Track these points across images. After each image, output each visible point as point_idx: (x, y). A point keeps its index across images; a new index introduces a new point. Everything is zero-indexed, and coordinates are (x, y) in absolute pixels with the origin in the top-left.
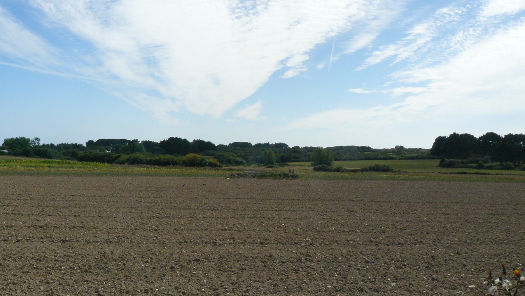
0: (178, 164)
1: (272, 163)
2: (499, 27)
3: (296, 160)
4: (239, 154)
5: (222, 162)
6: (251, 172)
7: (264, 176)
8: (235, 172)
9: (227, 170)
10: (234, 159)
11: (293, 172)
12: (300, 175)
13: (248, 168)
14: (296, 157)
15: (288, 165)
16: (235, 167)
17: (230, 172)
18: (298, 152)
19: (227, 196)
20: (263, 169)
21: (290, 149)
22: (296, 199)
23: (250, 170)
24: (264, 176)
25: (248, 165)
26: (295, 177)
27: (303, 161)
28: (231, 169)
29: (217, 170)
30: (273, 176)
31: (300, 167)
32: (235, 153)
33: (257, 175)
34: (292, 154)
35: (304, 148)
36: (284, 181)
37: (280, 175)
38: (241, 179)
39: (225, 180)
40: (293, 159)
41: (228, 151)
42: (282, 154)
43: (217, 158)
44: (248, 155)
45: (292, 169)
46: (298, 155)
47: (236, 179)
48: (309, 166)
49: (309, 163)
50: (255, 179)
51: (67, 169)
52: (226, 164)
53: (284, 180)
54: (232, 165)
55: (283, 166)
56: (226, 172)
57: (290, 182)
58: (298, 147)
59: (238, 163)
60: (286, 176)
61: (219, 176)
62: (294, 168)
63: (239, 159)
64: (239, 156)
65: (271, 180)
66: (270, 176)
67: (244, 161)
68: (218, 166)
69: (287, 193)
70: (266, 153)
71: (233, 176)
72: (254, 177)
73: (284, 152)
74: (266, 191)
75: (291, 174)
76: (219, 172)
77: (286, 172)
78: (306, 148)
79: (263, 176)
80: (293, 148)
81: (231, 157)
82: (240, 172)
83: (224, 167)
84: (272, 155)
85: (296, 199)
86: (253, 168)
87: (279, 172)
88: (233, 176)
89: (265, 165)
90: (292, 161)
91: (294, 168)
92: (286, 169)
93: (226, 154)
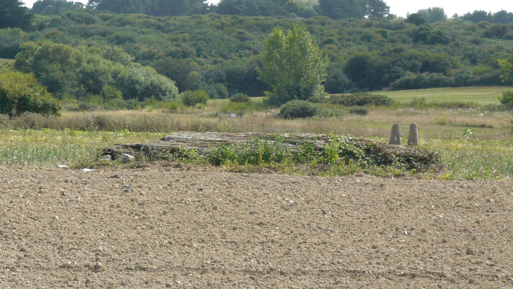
0: (132, 147)
1: (306, 94)
2: (35, 74)
3: (426, 76)
4: (144, 49)
5: (54, 87)
6: (199, 136)
7: (266, 158)
8: (122, 138)
9: (84, 127)
10: (115, 75)
11: (412, 140)
12: (445, 157)
13: (185, 118)
14: (428, 66)
15: (384, 103)
16: (123, 114)
17: (98, 140)
18: (438, 39)
19: (82, 257)
20: (258, 122)
21: (399, 25)
22: (427, 274)
23: (195, 128)
24: (266, 158)
25: (188, 102)
26: (420, 162)
27: (462, 83)
28: (101, 124)
29: (32, 126)
30: (315, 158)
31: (448, 114)
32: (120, 41)
33: (230, 150)
34: (409, 49)
35: (468, 17)
36: (366, 182)
37: (348, 155)
38: (154, 170)
39: (72, 175)
40: (412, 76)
41: (87, 35)
42: (361, 50)
43: (36, 66)
44: (185, 55)
45: (405, 122)
46: (431, 53)
47: (126, 175)
48: (491, 109)
49: (493, 96)
50: (222, 173)
51: (89, 115)
52: (78, 95)
53: (367, 178)
54: (107, 99)
55: (360, 106)
56: (79, 135)
57: (396, 186)
58: (437, 14)
59: (135, 93)
60: (379, 157)
61: (42, 157)
62: (414, 119)
63: (144, 74)
64: (146, 59)
65: (298, 177)
66: (297, 159)
67: (169, 84)
68: (36, 109)
69: (380, 242)
70: (275, 43)
71: (114, 155)
72: (217, 162)
73: (367, 38)
74: (275, 234)
75: (402, 147)
76: (41, 135)
77: (375, 140)
78: (479, 17)
79: (258, 160)
80: (413, 19)
81: (104, 64)
82: (149, 140)
83: (66, 115)
84: (304, 51)
85: (427, 274)
86: (216, 121)
87: (343, 138)
88: (114, 155)
89: (273, 103)
90: (407, 86)
91: (414, 119)
92: (374, 125)
93: (78, 50)
